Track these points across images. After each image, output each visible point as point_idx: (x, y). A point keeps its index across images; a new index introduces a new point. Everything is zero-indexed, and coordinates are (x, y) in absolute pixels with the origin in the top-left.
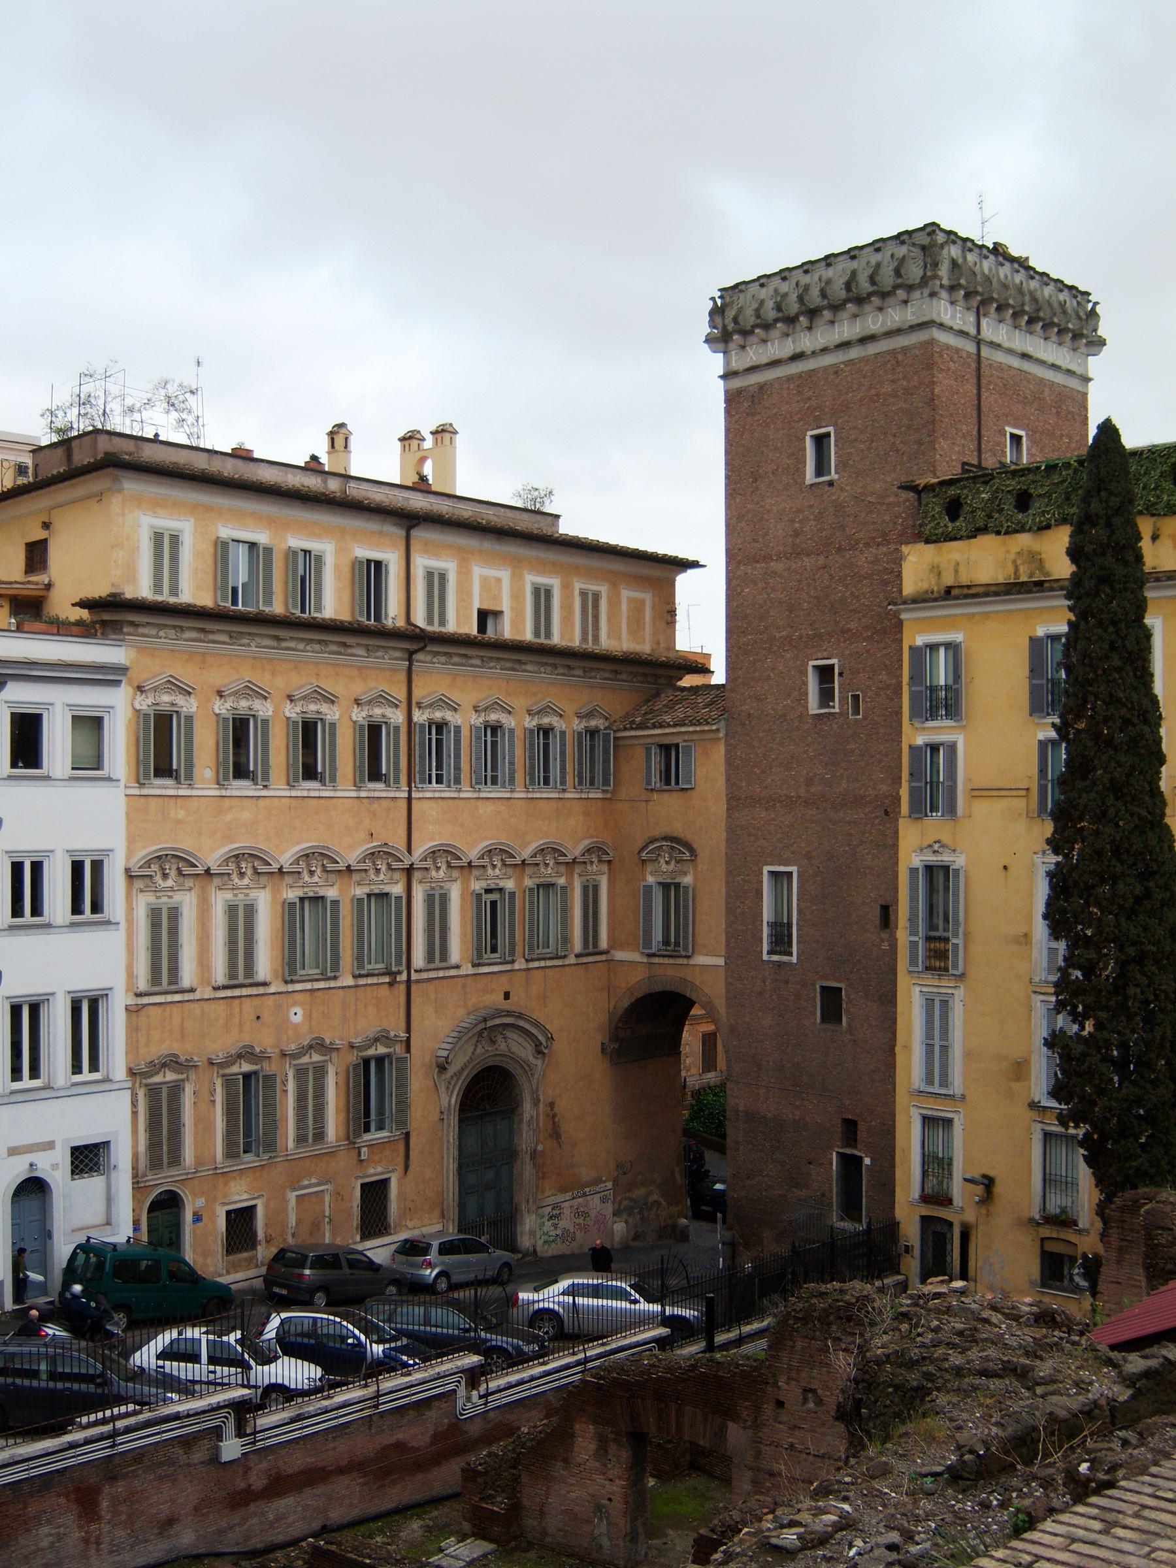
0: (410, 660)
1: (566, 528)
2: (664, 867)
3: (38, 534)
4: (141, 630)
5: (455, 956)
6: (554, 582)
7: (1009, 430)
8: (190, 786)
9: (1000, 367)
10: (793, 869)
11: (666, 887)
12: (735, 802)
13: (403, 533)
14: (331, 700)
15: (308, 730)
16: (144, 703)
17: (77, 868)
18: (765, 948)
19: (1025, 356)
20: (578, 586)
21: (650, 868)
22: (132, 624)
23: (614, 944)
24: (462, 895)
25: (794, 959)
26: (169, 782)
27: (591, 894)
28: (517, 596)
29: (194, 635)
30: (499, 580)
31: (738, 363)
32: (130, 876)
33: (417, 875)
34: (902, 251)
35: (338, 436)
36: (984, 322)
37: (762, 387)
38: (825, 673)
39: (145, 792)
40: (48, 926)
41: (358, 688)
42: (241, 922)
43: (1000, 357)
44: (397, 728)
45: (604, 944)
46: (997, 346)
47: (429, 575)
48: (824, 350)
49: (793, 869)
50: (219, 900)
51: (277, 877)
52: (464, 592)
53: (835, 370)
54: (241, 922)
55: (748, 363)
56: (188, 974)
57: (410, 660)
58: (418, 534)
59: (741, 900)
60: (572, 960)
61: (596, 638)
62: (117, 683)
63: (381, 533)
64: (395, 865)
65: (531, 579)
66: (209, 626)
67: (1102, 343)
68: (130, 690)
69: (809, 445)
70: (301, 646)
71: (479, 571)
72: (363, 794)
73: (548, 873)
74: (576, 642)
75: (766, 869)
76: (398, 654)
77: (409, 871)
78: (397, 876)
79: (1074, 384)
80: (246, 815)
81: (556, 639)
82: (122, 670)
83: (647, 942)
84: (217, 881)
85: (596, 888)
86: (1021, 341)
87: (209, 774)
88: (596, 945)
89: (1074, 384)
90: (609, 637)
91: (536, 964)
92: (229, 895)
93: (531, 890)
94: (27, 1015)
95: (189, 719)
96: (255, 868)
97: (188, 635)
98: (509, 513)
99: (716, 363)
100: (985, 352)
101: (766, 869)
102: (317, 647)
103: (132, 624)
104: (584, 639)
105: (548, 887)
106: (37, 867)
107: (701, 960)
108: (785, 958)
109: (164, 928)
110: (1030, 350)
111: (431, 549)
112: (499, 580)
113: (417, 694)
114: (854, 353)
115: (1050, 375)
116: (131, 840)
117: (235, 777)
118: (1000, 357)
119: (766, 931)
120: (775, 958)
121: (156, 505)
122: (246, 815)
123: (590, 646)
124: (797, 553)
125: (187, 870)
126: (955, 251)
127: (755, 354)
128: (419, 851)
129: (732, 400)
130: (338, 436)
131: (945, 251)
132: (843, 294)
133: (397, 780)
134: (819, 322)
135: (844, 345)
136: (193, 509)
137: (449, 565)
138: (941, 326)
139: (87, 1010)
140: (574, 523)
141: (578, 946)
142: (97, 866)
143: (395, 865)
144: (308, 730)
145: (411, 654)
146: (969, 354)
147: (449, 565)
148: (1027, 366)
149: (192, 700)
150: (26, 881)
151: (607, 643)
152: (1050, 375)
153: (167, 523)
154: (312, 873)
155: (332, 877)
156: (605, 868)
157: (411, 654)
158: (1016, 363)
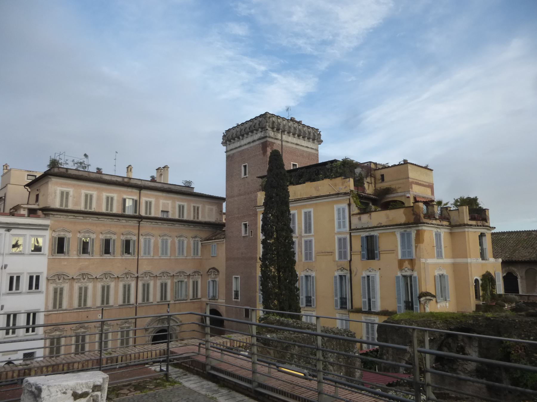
0: (139, 223)
1: (196, 191)
2: (212, 276)
3: (38, 193)
4: (55, 216)
5: (169, 298)
6: (185, 204)
7: (292, 163)
8: (69, 256)
9: (289, 147)
10: (239, 276)
11: (213, 281)
12: (228, 259)
13: (139, 192)
14: (115, 234)
15: (107, 242)
16: (56, 235)
17: (31, 278)
18: (233, 297)
19: (297, 144)
20: (192, 205)
21: (210, 276)
22: (52, 214)
23: (202, 296)
24: (171, 283)
25: (239, 300)
26: (108, 255)
27: (195, 284)
28: (174, 208)
29: (72, 217)
30: (168, 204)
31: (229, 149)
32: (48, 280)
33: (140, 279)
34: (260, 119)
35: (129, 168)
36: (284, 136)
37: (233, 154)
38: (245, 225)
39: (54, 257)
40: (20, 293)
41: (123, 230)
42: (164, 287)
43: (289, 145)
44: (134, 241)
45: (199, 295)
46: (288, 142)
47: (146, 202)
48: (245, 145)
49: (239, 276)
50: (76, 286)
51: (95, 280)
52: (157, 205)
53: (247, 149)
54: (164, 287)
55: (231, 148)
56: (151, 299)
57: (139, 223)
58: (142, 192)
59: (229, 284)
60: (189, 301)
61: (198, 218)
62: (47, 229)
63: (132, 192)
64: (132, 276)
65: (178, 203)
66: (76, 215)
67: (322, 141)
68: (51, 231)
69: (243, 168)
70: (106, 220)
71: (161, 201)
72: (123, 258)
73: (182, 278)
74: (191, 219)
75: (234, 276)
76: (136, 222)
77: (137, 277)
78: (134, 279)
79: (313, 151)
80: (86, 263)
81: (185, 218)
82: (47, 226)
83: (209, 297)
84: (76, 281)
85: (197, 282)
86: (295, 140)
87: (75, 253)
88: (197, 296)
89: (313, 151)
90: (202, 217)
91: (177, 302)
92: (80, 284)
93: (176, 282)
94: (12, 317)
95: (69, 239)
96: (64, 279)
97: (70, 217)
98: (179, 187)
99: (224, 148)
100: (284, 143)
101: (234, 276)
102: (110, 220)
103: (52, 214)
104: (194, 218)
105: (182, 281)
106: (18, 278)
107: (220, 301)
108: (237, 300)
109: (58, 294)
110: (299, 143)
111: (146, 196)
112: (168, 204)
113: (141, 232)
114: (252, 145)
115: (306, 149)
116: (49, 270)
117: (83, 253)
118: (289, 145)
119: (233, 293)
120: (235, 300)
121: (61, 185)
122: (86, 263)
123: (196, 220)
124: (240, 195)
125: (66, 278)
126: (274, 119)
127: (232, 146)
128: (140, 272)
129: (228, 157)
130: (129, 168)
131: (271, 119)
132: (249, 130)
133: (134, 254)
134: (245, 138)
135: (249, 143)
136: (74, 186)
137: (153, 200)
138: (270, 137)
139: (31, 316)
140: (197, 190)
141: (191, 297)
142: (38, 278)
143: (132, 276)
144: (107, 242)
145: (139, 222)
146: (279, 144)
147: (153, 200)
148: (298, 147)
149: (71, 233)
150: (13, 283)
151: (201, 219)
152: (306, 149)
153: (65, 189)
154: (106, 278)
155: (113, 279)
156: (200, 276)
157: (139, 222)
158: (294, 146)
